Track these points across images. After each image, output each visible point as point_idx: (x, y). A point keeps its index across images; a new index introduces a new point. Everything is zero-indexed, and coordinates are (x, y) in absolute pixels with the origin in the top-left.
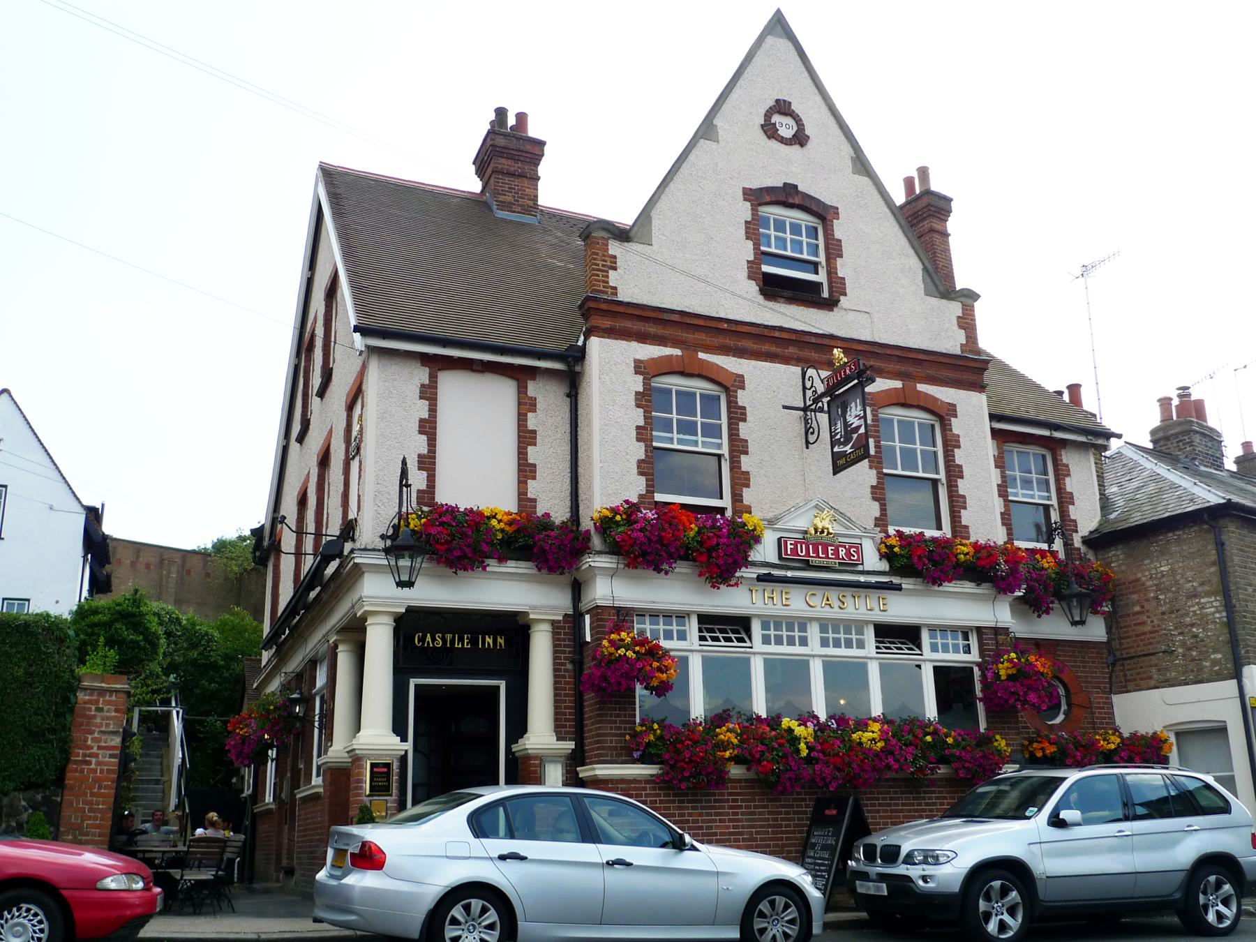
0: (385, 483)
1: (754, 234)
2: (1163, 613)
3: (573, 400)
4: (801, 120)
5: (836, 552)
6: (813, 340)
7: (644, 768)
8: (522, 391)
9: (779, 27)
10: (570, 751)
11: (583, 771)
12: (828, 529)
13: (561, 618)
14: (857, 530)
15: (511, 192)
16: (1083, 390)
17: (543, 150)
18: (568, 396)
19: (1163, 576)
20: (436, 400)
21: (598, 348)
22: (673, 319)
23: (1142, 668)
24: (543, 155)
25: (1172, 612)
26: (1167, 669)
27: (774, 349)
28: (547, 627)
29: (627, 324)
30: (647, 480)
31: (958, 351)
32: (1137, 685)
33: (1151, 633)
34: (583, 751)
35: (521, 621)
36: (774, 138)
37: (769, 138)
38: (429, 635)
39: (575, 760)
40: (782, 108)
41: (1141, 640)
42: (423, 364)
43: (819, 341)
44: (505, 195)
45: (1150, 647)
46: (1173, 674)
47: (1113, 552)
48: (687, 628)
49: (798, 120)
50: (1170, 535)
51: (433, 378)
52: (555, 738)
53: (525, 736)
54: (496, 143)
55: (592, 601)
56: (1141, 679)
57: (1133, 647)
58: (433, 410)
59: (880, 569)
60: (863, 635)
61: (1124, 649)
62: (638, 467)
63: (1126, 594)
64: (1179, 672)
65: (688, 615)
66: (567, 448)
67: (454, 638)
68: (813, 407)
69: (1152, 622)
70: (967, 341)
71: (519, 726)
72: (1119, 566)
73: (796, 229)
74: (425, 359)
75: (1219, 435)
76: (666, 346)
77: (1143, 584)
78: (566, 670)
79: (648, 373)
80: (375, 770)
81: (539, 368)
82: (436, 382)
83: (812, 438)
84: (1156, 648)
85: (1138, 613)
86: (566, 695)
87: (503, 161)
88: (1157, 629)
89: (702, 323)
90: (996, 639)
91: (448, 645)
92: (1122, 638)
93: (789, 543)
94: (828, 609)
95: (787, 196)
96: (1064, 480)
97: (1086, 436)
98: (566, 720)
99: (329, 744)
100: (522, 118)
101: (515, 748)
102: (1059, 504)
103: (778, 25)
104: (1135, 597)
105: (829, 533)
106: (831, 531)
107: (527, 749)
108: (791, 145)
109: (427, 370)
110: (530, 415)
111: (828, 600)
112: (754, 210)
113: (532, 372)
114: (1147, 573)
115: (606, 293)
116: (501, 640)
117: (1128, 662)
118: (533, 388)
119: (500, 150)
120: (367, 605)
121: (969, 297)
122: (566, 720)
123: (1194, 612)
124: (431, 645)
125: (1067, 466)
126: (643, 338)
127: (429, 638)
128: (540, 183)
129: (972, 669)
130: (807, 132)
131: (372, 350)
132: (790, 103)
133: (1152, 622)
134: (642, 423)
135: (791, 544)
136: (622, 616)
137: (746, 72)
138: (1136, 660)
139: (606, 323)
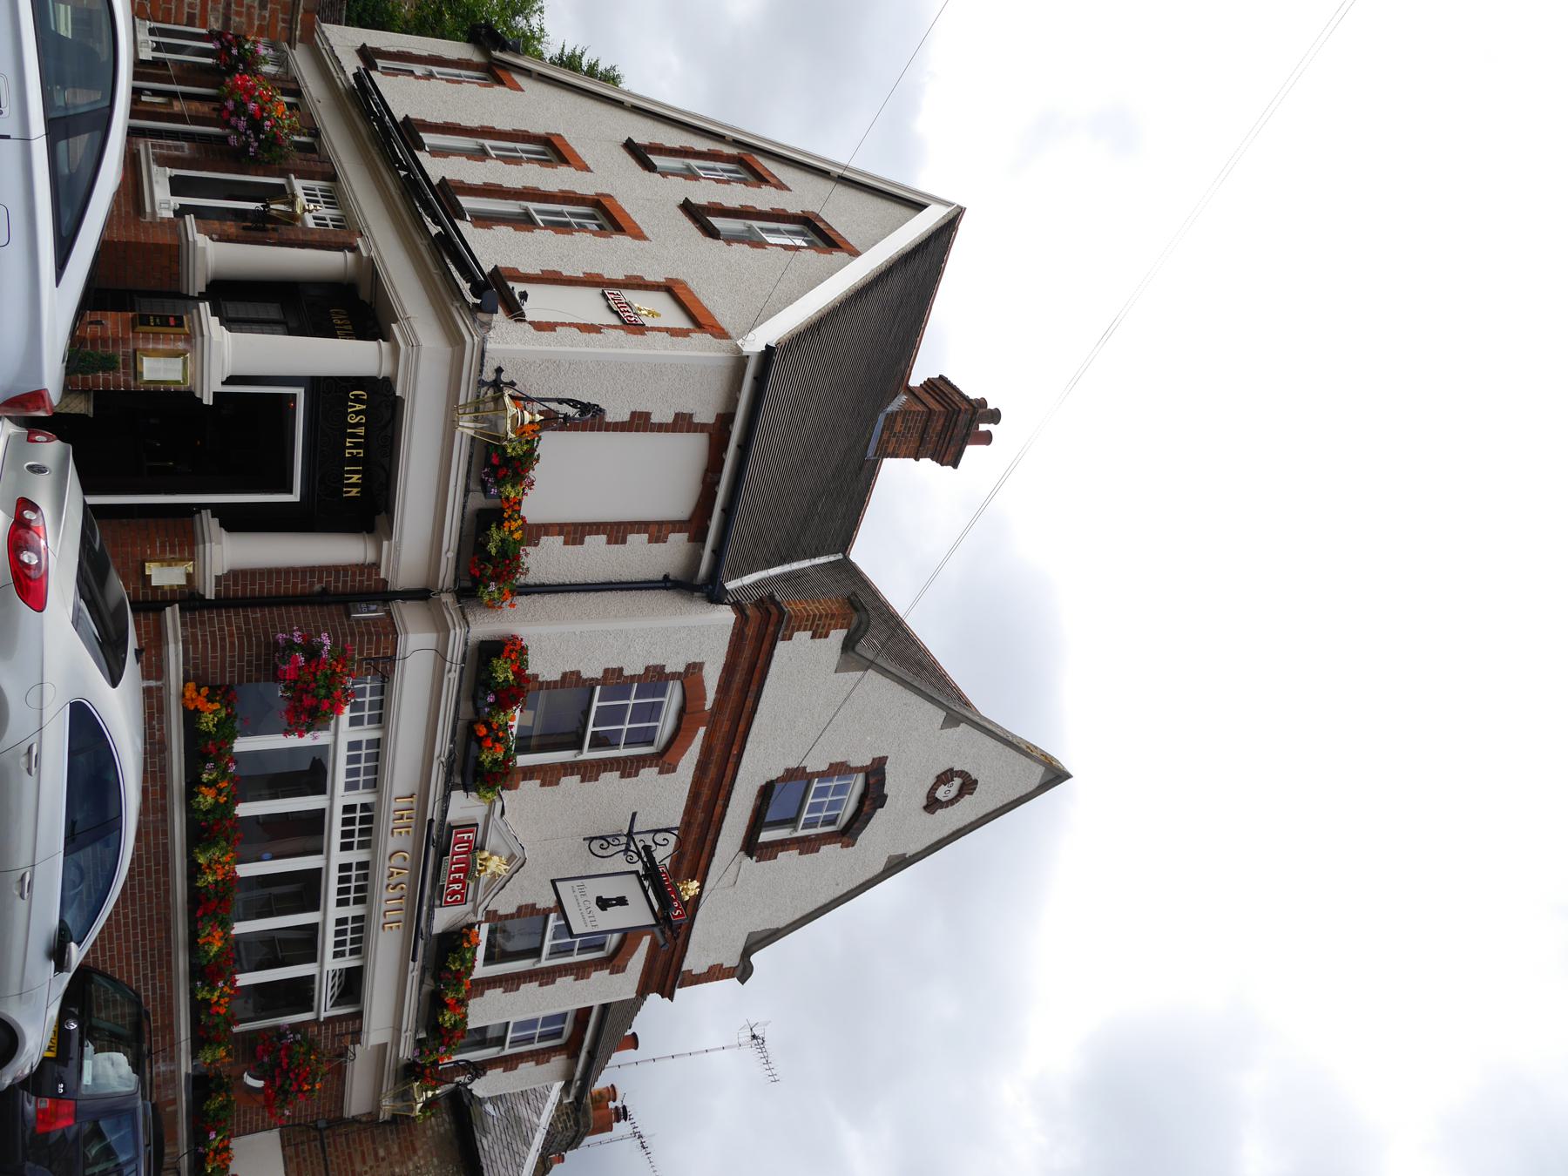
0: (570, 372)
1: (835, 772)
3: (660, 585)
4: (952, 804)
5: (456, 881)
6: (710, 837)
8: (675, 526)
9: (1051, 776)
10: (202, 593)
12: (486, 870)
13: (382, 576)
14: (482, 898)
15: (905, 429)
16: (632, 1051)
17: (947, 465)
18: (666, 577)
20: (674, 431)
21: (724, 616)
22: (748, 699)
23: (312, 1163)
24: (942, 465)
27: (703, 799)
28: (371, 557)
29: (747, 653)
30: (555, 682)
31: (685, 968)
32: (291, 1159)
35: (380, 520)
36: (937, 781)
37: (938, 777)
38: (365, 407)
39: (189, 599)
40: (969, 785)
41: (344, 1160)
42: (720, 417)
43: (708, 843)
44: (902, 423)
45: (332, 1150)
47: (447, 1120)
48: (366, 726)
49: (952, 802)
51: (700, 428)
53: (223, 530)
54: (961, 415)
56: (298, 1164)
57: (336, 1150)
58: (661, 428)
60: (369, 723)
61: (334, 1141)
62: (572, 673)
63: (398, 1138)
65: (377, 792)
66: (601, 577)
67: (360, 437)
68: (633, 848)
70: (694, 975)
71: (237, 521)
72: (432, 1128)
73: (835, 805)
74: (726, 419)
75: (576, 1147)
76: (716, 692)
77: (410, 1159)
78: (312, 584)
79: (686, 677)
81: (703, 548)
82: (695, 431)
83: (595, 845)
85: (376, 1154)
86: (278, 584)
89: (741, 728)
90: (347, 1033)
91: (349, 431)
93: (471, 835)
94: (387, 873)
95: (873, 797)
96: (532, 1061)
97: (580, 1079)
98: (244, 586)
99: (215, 236)
100: (987, 438)
101: (206, 514)
102: (505, 1056)
103: (1055, 775)
104: (395, 1149)
105: (480, 872)
106: (482, 874)
107: (204, 543)
108: (928, 798)
109: (712, 421)
110: (645, 537)
111: (398, 873)
112: (846, 558)
113: (698, 536)
114: (422, 1162)
115: (786, 629)
116: (354, 492)
117: (319, 1146)
118: (678, 541)
119: (954, 419)
120: (407, 351)
121: (743, 972)
122: (244, 586)
124: (349, 410)
125: (548, 1061)
126: (729, 669)
127: (359, 407)
128: (912, 460)
129: (310, 1009)
130: (939, 811)
131: (741, 361)
132: (971, 794)
134: (626, 673)
135: (469, 837)
136: (384, 667)
137: (1010, 750)
138: (321, 1156)
139: (750, 631)
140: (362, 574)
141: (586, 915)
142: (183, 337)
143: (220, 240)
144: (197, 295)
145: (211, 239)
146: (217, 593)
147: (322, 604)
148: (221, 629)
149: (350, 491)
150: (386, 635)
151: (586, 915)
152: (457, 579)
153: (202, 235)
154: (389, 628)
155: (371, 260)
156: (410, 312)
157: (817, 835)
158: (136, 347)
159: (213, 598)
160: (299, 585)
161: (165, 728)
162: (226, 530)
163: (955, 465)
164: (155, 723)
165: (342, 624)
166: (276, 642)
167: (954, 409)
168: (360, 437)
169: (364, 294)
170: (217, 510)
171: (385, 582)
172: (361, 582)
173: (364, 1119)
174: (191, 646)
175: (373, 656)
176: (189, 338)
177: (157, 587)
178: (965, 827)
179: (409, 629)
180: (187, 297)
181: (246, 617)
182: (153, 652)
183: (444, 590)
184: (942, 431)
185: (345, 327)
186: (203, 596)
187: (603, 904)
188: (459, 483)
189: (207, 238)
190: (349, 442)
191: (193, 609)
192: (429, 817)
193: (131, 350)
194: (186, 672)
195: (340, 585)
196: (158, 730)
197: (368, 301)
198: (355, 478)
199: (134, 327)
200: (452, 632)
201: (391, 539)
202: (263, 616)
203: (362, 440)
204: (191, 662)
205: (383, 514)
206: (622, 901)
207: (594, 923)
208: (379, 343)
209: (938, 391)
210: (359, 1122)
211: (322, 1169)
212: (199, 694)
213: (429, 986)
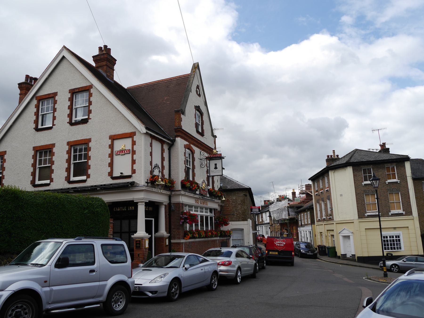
2: (233, 207)
7: (184, 240)
11: (172, 241)
13: (167, 204)
18: (168, 149)
19: (234, 200)
25: (235, 207)
26: (233, 218)
28: (164, 206)
33: (230, 210)
35: (156, 204)
45: (225, 213)
46: (234, 219)
50: (236, 192)
52: (166, 233)
53: (158, 232)
55: (179, 201)
64: (235, 219)
67: (122, 208)
69: (230, 208)
77: (229, 201)
80: (137, 242)
84: (231, 214)
87: (108, 62)
88: (231, 210)
92: (223, 211)
104: (227, 203)
114: (230, 199)
116: (133, 208)
123: (239, 207)
129: (212, 217)
131: (147, 133)
133: (230, 208)
141: (218, 172)
148: (176, 233)
150: (180, 205)
151: (218, 172)
157: (201, 120)
163: (116, 60)
167: (106, 59)
170: (155, 234)
173: (221, 208)
178: (202, 88)
179: (179, 201)
181: (173, 229)
184: (110, 63)
186: (169, 236)
187: (216, 168)
192: (199, 197)
199: (140, 249)
200: (182, 193)
202: (173, 226)
206: (216, 165)
207: (220, 171)
209: (99, 60)
210: (221, 208)
211: (228, 215)
213: (188, 190)
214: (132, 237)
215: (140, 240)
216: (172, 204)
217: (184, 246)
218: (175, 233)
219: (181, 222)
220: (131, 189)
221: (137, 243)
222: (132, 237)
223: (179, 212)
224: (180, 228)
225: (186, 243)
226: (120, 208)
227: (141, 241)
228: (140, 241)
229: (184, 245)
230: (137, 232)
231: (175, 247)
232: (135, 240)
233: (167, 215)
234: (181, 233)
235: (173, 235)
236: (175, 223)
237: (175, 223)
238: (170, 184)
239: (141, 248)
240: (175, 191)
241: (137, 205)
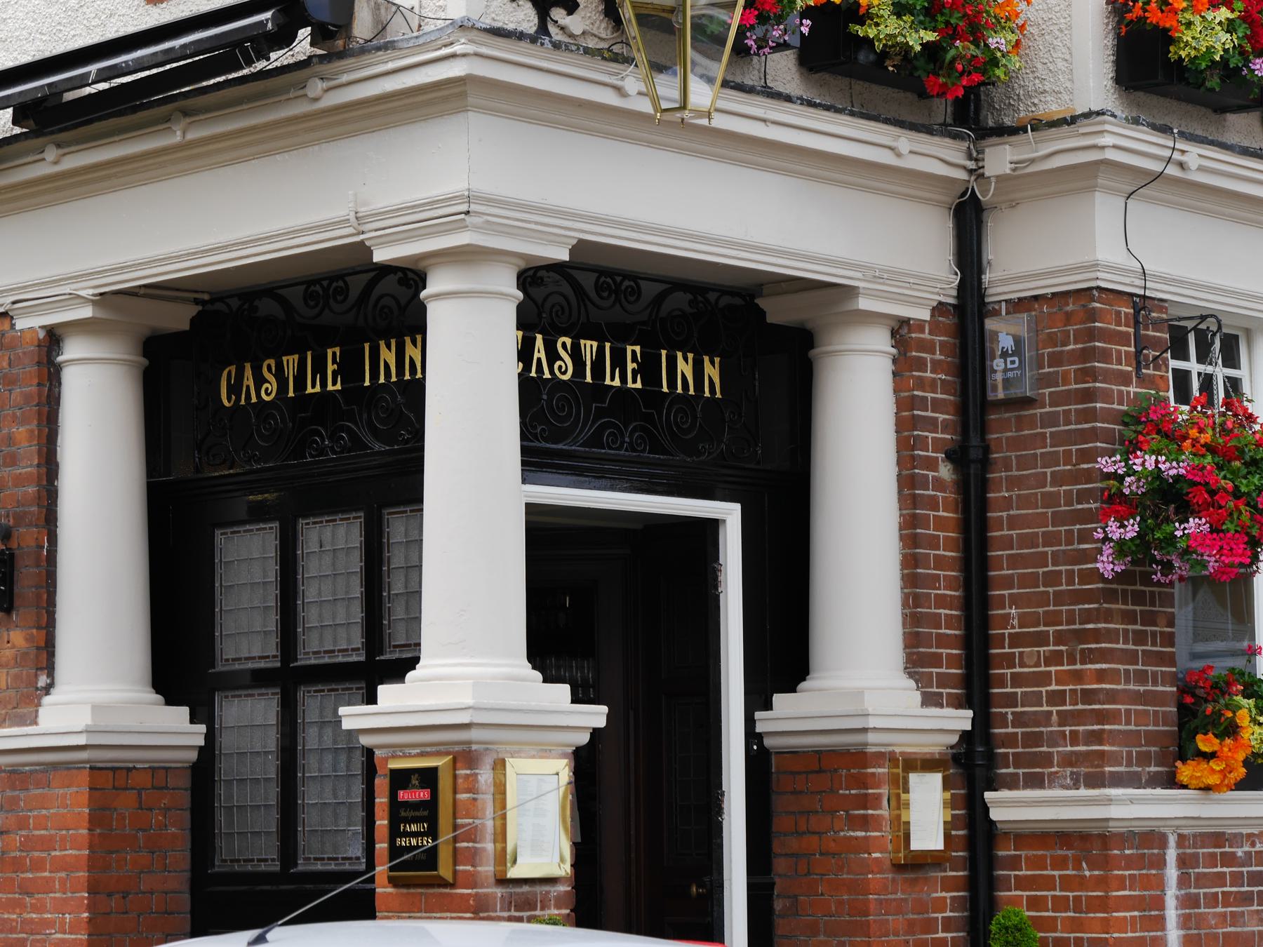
10: (954, 739)
13: (925, 315)
28: (879, 341)
34: (988, 740)
35: (777, 311)
38: (539, 337)
52: (918, 696)
53: (417, 666)
59: (351, 233)
78: (939, 484)
80: (403, 795)
91: (589, 379)
99: (43, 681)
101: (765, 723)
116: (712, 371)
120: (476, 228)
124: (547, 375)
140: (921, 364)
142: (462, 772)
143: (50, 669)
144: (202, 728)
145: (48, 689)
146: (958, 704)
147: (985, 463)
149: (386, 363)
150: (1092, 315)
152: (943, 131)
153: (41, 710)
154: (1070, 308)
155: (104, 300)
156: (342, 210)
158: (492, 880)
159: (970, 713)
160: (941, 513)
161: (1249, 831)
162: (804, 680)
164: (1240, 852)
165: (1051, 420)
166: (1119, 577)
168: (601, 350)
169: (178, 318)
170: (757, 698)
171: (939, 309)
172: (936, 366)
174: (1107, 769)
175: (1133, 349)
176: (466, 757)
177: (948, 838)
179: (1086, 258)
180: (208, 752)
181: (1016, 640)
182: (1116, 852)
183: (971, 165)
185: (291, 373)
188: (759, 112)
189: (47, 700)
190: (613, 379)
191: (992, 760)
193: (499, 891)
194: (1154, 781)
195: (941, 417)
196: (1253, 845)
197: (193, 310)
198: (685, 367)
201: (855, 288)
202: (1015, 601)
203: (608, 345)
204: (1135, 769)
205: (760, 302)
208: (437, 296)
212: (1213, 755)
214: (347, 725)
215: (434, 771)
216: (996, 313)
217: (1172, 873)
218: (1036, 699)
219: (1108, 550)
220: (317, 87)
221: (406, 805)
222: (347, 725)
223: (1090, 415)
224: (1096, 636)
225: (1218, 839)
226: (280, 366)
227: (444, 783)
228: (429, 777)
229: (1183, 862)
230: (422, 662)
231: (1048, 883)
232: (386, 760)
233: (931, 464)
234: (1112, 697)
235: (1019, 720)
236: (1041, 560)
237: (1041, 560)
238: (914, 27)
239: (445, 871)
240: (1003, 131)
241: (422, 309)
